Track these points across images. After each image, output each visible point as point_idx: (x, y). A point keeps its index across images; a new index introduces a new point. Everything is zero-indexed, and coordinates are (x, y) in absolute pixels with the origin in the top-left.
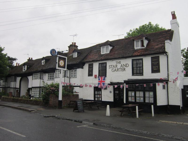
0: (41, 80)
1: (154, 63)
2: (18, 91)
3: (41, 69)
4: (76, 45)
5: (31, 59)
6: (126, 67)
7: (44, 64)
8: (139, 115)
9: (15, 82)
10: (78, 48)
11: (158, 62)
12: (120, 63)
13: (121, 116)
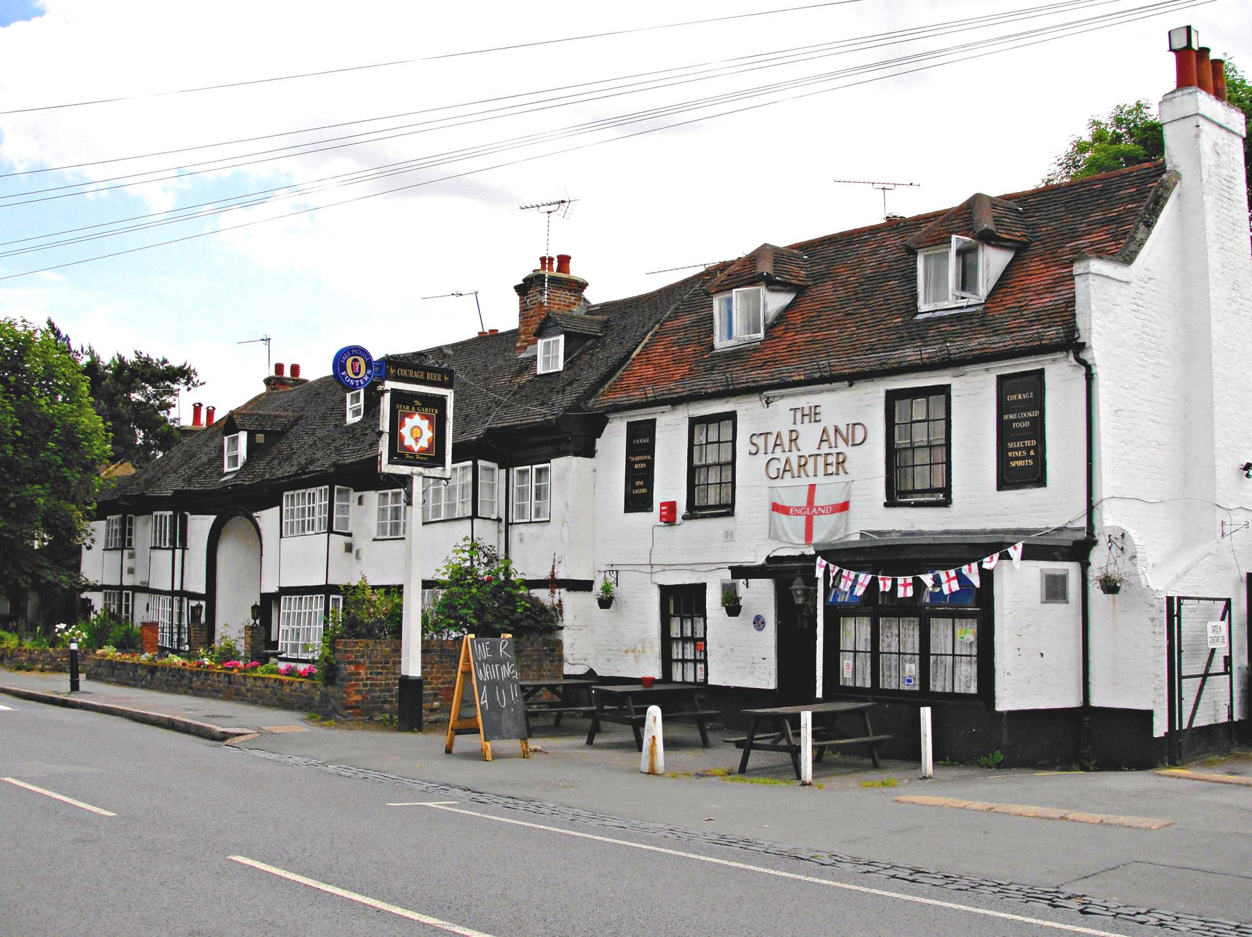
0: (331, 535)
1: (1012, 417)
2: (203, 619)
3: (334, 458)
4: (576, 271)
5: (287, 373)
6: (854, 445)
7: (358, 419)
8: (817, 760)
9: (178, 552)
10: (586, 294)
11: (1037, 413)
12: (813, 415)
13: (743, 769)
